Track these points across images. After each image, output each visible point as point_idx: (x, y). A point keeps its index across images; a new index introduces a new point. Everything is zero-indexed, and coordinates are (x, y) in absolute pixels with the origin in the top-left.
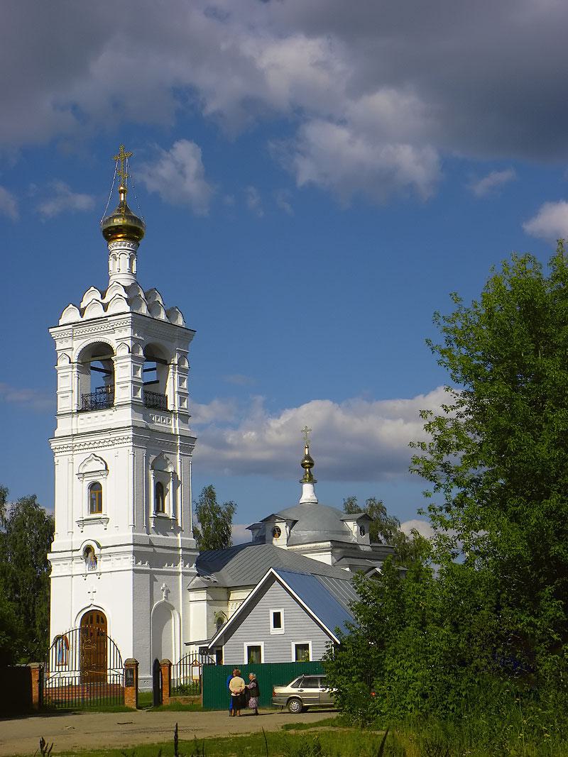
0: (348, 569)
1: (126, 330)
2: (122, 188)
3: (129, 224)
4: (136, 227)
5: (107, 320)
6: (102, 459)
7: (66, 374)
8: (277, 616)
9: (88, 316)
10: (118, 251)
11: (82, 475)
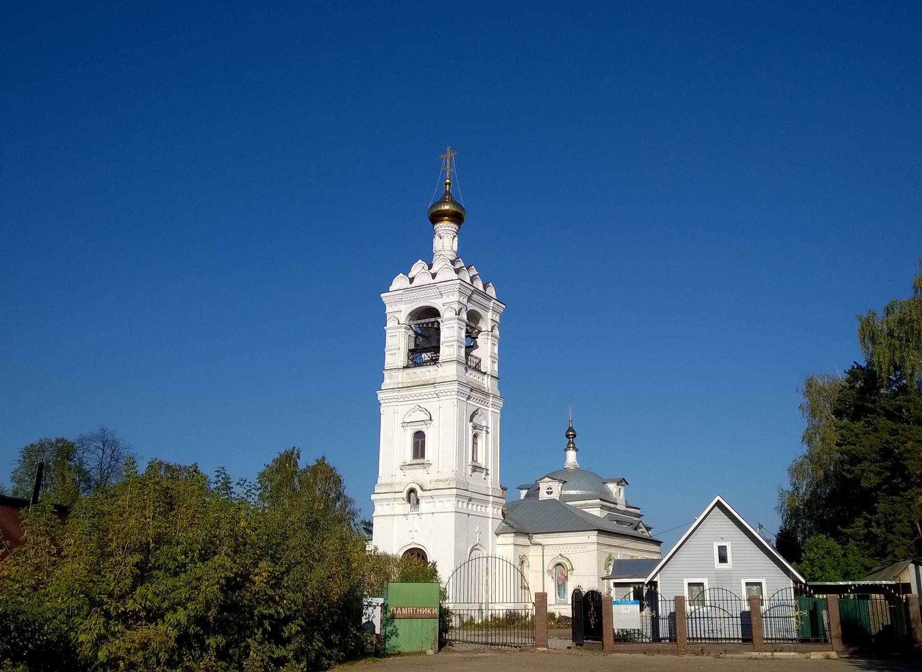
0: (615, 523)
1: (453, 295)
2: (448, 181)
3: (451, 209)
4: (460, 213)
5: (436, 286)
6: (426, 410)
7: (394, 334)
8: (722, 550)
9: (415, 283)
10: (443, 231)
11: (405, 424)
